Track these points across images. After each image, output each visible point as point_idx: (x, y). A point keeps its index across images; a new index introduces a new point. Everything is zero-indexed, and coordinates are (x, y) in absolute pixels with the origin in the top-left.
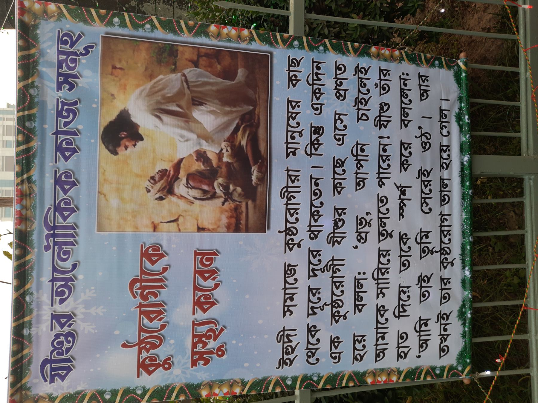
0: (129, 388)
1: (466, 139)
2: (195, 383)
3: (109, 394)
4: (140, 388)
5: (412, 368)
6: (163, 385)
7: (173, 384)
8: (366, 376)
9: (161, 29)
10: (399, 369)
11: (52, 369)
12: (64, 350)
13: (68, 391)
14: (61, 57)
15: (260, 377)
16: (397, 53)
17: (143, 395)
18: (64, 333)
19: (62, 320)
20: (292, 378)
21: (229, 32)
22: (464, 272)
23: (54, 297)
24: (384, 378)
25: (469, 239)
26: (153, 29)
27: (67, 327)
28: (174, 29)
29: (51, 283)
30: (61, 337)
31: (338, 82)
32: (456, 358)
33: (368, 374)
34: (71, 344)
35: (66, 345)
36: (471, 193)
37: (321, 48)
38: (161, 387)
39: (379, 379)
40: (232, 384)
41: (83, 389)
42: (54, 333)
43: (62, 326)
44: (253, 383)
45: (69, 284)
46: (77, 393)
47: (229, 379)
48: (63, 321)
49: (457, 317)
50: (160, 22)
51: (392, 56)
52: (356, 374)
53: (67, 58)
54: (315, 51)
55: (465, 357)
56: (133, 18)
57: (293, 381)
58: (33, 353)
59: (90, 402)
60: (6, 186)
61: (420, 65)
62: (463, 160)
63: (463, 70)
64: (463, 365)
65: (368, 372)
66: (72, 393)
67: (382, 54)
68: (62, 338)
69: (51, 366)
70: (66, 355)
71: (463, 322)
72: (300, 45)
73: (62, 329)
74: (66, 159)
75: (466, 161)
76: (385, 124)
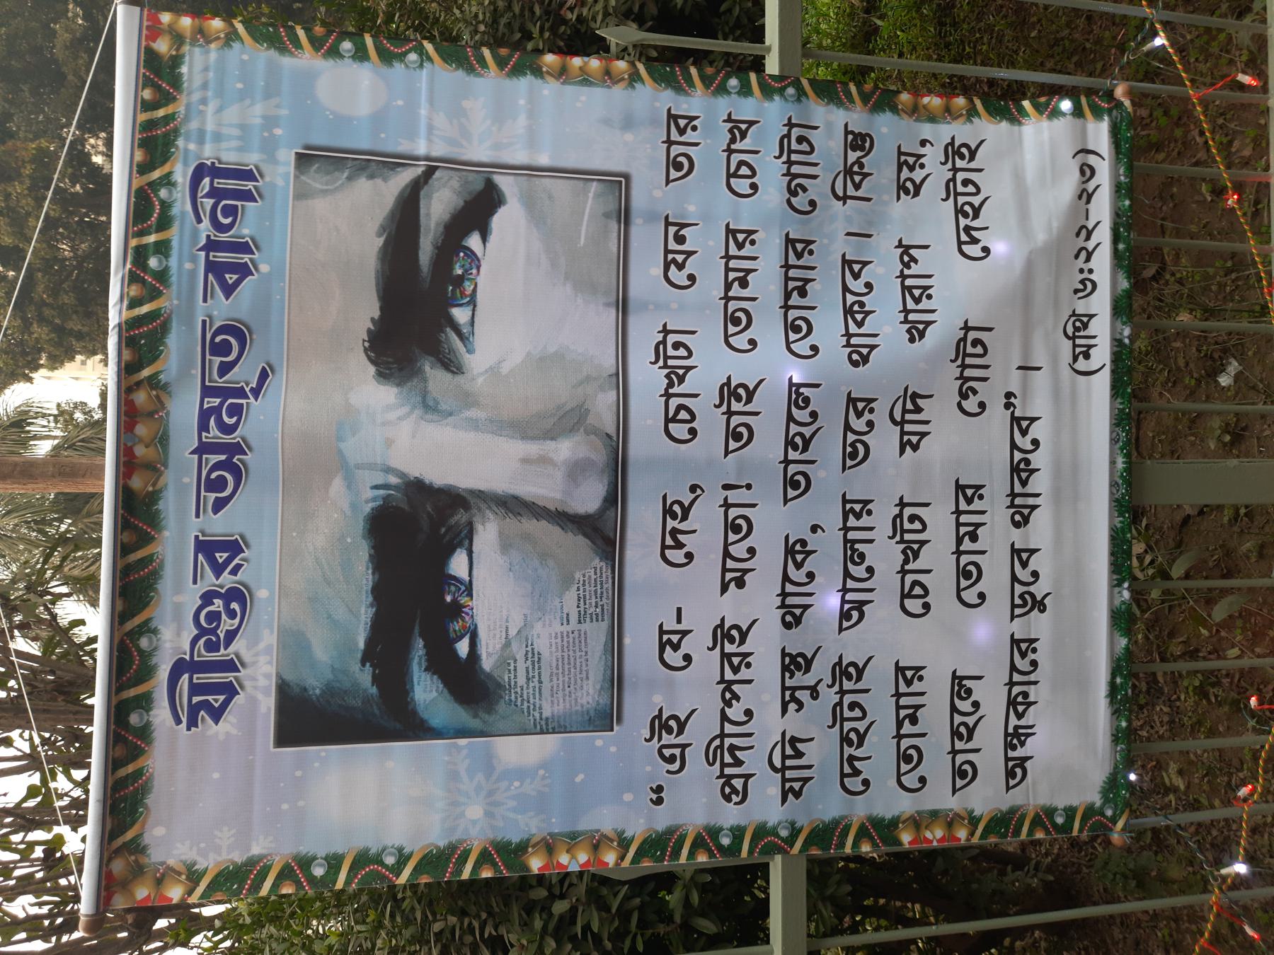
0: (367, 850)
2: (515, 839)
3: (321, 865)
4: (393, 850)
5: (1001, 811)
6: (442, 843)
7: (465, 841)
8: (898, 827)
9: (311, 48)
11: (195, 689)
12: (222, 636)
13: (230, 857)
14: (208, 402)
17: (398, 868)
18: (223, 591)
19: (227, 276)
23: (203, 493)
24: (939, 833)
26: (422, 61)
27: (230, 573)
28: (839, 99)
29: (196, 457)
30: (215, 601)
32: (1099, 789)
33: (904, 822)
34: (237, 621)
39: (928, 835)
40: (597, 843)
41: (264, 852)
42: (202, 587)
43: (218, 569)
44: (644, 842)
45: (235, 460)
46: (251, 862)
47: (591, 831)
48: (221, 557)
53: (222, 404)
54: (777, 98)
58: (153, 768)
59: (278, 882)
61: (684, 90)
66: (239, 861)
68: (218, 604)
69: (191, 679)
70: (225, 649)
72: (742, 86)
73: (217, 579)
74: (229, 290)
76: (911, 163)
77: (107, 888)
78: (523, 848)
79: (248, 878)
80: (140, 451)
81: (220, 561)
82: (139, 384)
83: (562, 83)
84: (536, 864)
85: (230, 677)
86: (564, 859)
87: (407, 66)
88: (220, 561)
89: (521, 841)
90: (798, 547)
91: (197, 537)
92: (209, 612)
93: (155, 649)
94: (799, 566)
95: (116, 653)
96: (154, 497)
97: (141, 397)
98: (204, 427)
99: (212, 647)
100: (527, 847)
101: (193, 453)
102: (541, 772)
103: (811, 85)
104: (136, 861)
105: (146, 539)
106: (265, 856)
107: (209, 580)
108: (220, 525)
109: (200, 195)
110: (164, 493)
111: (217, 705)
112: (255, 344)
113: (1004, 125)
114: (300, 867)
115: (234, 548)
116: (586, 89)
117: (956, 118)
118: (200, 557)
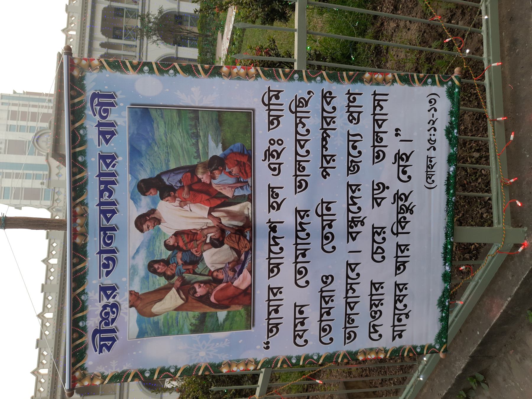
0: (164, 367)
1: (454, 151)
2: (217, 362)
5: (396, 348)
6: (191, 364)
10: (386, 348)
11: (101, 339)
12: (110, 320)
15: (270, 357)
16: (390, 76)
18: (110, 304)
20: (296, 357)
21: (239, 71)
22: (445, 267)
23: (102, 268)
25: (450, 239)
26: (175, 73)
31: (351, 99)
32: (434, 339)
35: (112, 316)
36: (454, 200)
37: (319, 78)
38: (189, 366)
41: (128, 368)
43: (108, 297)
46: (124, 372)
48: (109, 292)
49: (437, 305)
50: (181, 67)
51: (384, 80)
52: (350, 353)
54: (313, 81)
55: (442, 338)
56: (159, 66)
57: (297, 359)
60: (6, 169)
62: (449, 170)
63: (457, 86)
64: (440, 344)
65: (359, 351)
67: (375, 79)
68: (108, 309)
69: (100, 336)
71: (441, 309)
73: (108, 300)
74: (107, 141)
75: (452, 171)
77: (74, 216)
78: (220, 365)
79: (122, 377)
80: (79, 229)
81: (109, 294)
82: (77, 204)
83: (230, 79)
84: (225, 370)
85: (113, 335)
86: (235, 369)
87: (169, 75)
88: (109, 294)
89: (219, 363)
90: (328, 95)
91: (99, 154)
92: (106, 312)
93: (87, 300)
94: (328, 104)
95: (72, 302)
96: (85, 245)
97: (78, 209)
98: (101, 196)
99: (107, 324)
100: (221, 365)
101: (97, 206)
102: (227, 340)
103: (327, 75)
104: (83, 373)
105: (82, 261)
106: (128, 370)
107: (105, 301)
108: (108, 281)
109: (94, 105)
110: (86, 77)
111: (109, 345)
112: (119, 262)
113: (406, 86)
114: (141, 373)
115: (113, 158)
116: (239, 81)
117: (251, 78)
118: (101, 161)
